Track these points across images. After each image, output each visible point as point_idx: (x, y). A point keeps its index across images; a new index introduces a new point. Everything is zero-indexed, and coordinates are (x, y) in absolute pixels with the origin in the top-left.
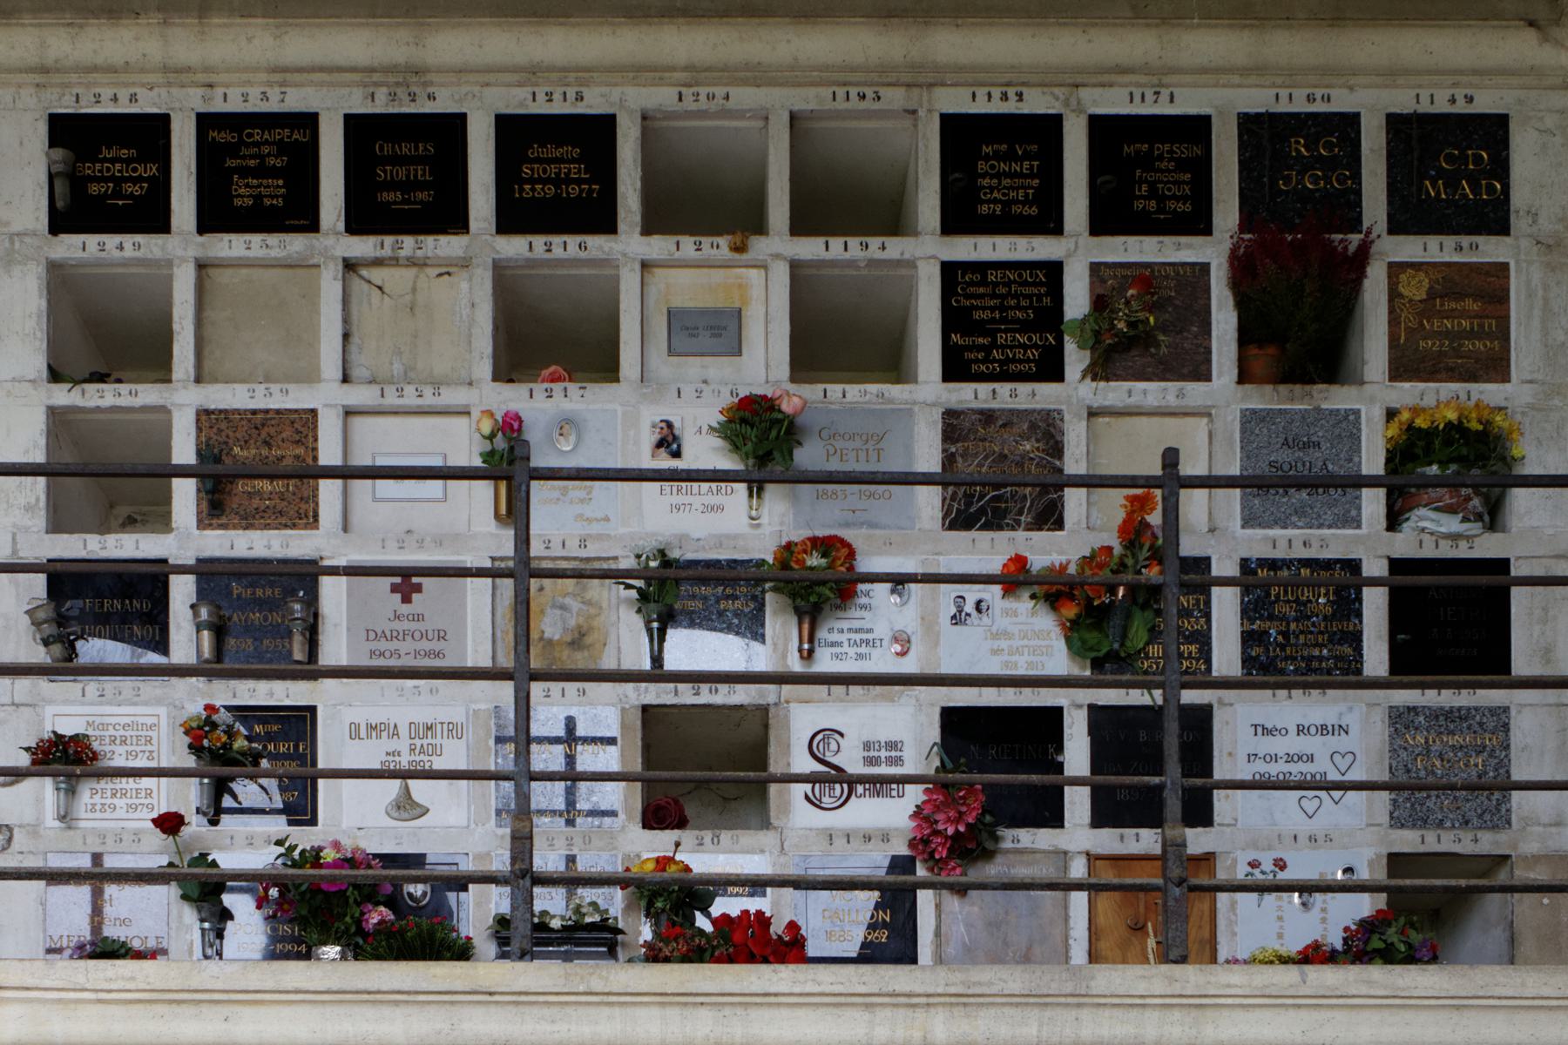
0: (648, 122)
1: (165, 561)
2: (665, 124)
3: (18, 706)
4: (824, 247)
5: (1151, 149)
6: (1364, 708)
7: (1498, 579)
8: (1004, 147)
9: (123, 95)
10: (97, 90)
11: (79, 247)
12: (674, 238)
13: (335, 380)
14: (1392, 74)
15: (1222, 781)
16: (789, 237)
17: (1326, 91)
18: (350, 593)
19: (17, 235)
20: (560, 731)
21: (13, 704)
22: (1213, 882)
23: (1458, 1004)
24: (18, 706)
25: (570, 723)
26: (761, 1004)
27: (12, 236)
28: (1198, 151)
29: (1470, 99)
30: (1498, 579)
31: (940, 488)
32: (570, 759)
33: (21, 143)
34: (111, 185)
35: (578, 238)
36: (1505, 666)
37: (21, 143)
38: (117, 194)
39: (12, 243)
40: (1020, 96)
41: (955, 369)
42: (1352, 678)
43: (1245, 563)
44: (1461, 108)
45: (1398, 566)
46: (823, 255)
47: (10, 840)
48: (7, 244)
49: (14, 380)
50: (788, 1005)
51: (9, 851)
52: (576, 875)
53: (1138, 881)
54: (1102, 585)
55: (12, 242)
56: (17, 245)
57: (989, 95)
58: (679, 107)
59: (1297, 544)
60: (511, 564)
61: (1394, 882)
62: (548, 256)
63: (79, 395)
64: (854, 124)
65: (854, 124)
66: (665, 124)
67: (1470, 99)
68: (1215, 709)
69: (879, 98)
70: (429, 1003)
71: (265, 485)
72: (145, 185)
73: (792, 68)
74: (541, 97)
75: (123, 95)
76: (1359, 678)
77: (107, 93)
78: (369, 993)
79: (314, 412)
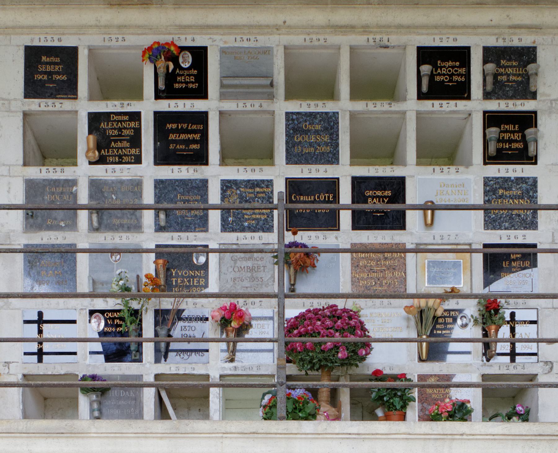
0: (288, 51)
1: (535, 246)
2: (363, 51)
3: (555, 309)
4: (366, 105)
9: (56, 37)
10: (124, 36)
11: (34, 104)
12: (366, 102)
13: (414, 165)
16: (349, 101)
17: (454, 36)
18: (90, 260)
19: (554, 100)
20: (36, 318)
21: (553, 308)
22: (140, 383)
23: (317, 435)
24: (555, 309)
25: (40, 314)
26: (317, 438)
27: (551, 101)
29: (520, 40)
31: (154, 211)
32: (40, 332)
33: (555, 60)
37: (555, 60)
39: (552, 104)
46: (431, 109)
47: (551, 368)
48: (549, 105)
49: (552, 164)
50: (231, 438)
51: (552, 373)
52: (142, 383)
53: (68, 382)
54: (302, 252)
55: (552, 104)
56: (554, 105)
58: (305, 44)
59: (512, 237)
60: (276, 247)
61: (484, 383)
62: (440, 109)
63: (170, 171)
64: (303, 51)
65: (303, 51)
66: (363, 51)
69: (125, 40)
70: (282, 438)
71: (257, 210)
74: (114, 40)
76: (129, 293)
77: (49, 38)
78: (373, 434)
79: (338, 179)
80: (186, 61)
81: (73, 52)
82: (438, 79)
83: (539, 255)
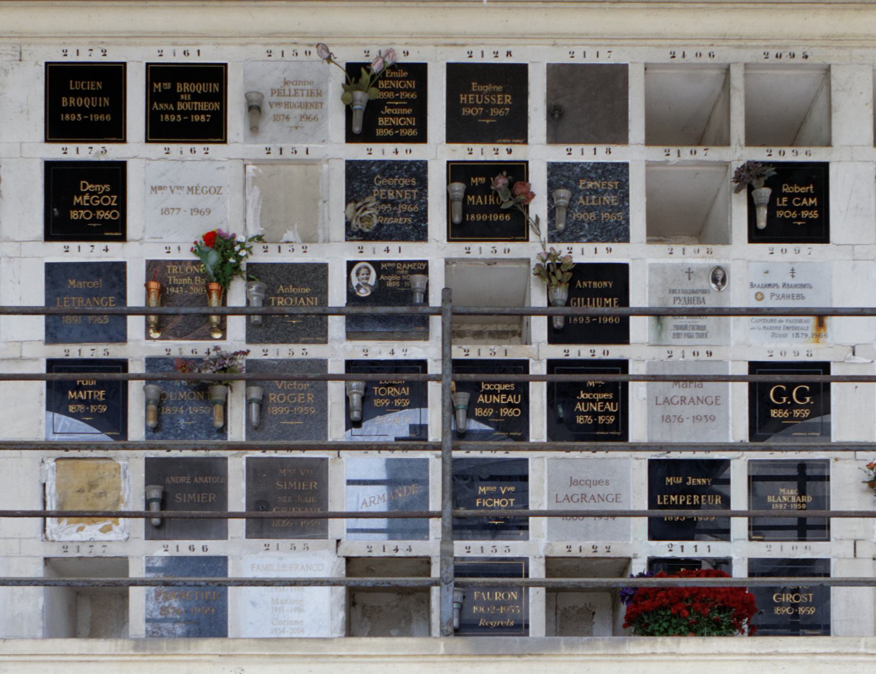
4: (593, 152)
5: (174, 87)
6: (53, 464)
7: (119, 376)
9: (180, 50)
14: (554, 39)
15: (535, 511)
26: (130, 661)
28: (216, 87)
30: (119, 376)
34: (482, 109)
35: (189, 146)
36: (625, 437)
38: (486, 115)
40: (767, 57)
41: (621, 234)
42: (423, 443)
43: (754, 367)
44: (503, 59)
45: (52, 364)
57: (684, 56)
68: (831, 464)
72: (508, 109)
73: (828, 37)
75: (193, 50)
81: (619, 73)
82: (780, 214)
83: (835, 388)
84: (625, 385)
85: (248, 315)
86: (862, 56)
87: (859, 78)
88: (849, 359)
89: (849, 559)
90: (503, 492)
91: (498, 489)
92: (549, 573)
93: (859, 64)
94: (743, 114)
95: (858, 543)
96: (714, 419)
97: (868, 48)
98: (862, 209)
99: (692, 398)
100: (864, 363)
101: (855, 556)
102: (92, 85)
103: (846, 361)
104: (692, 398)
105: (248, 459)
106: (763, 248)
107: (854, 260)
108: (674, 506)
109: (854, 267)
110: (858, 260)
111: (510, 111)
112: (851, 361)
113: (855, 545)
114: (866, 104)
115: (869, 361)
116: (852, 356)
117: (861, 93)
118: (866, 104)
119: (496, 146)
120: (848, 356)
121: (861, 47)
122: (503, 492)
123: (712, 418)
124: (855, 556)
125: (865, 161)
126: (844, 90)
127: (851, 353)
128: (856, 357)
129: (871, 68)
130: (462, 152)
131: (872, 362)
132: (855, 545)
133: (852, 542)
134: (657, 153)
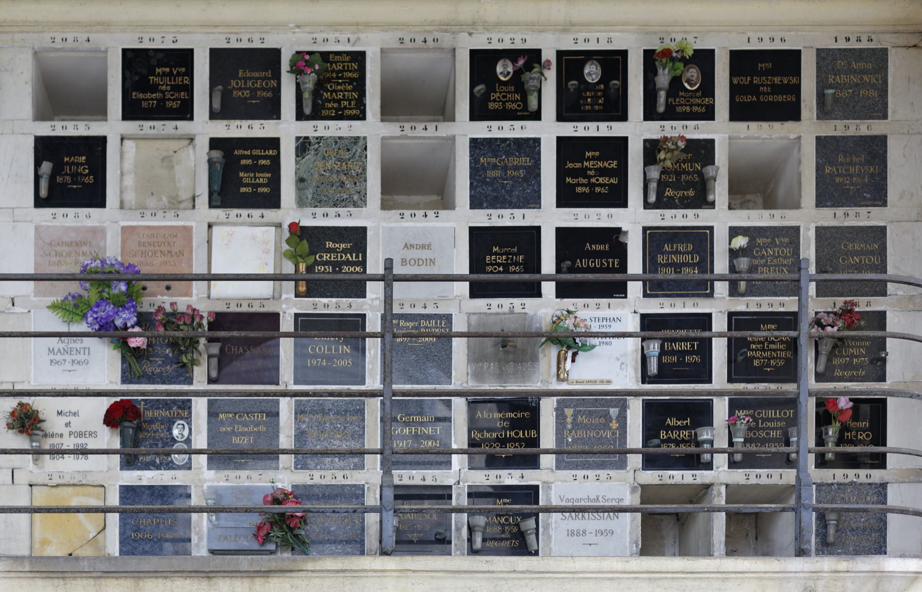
8: (168, 70)
9: (256, 37)
67: (610, 41)
72: (179, 102)
80: (592, 72)
81: (359, 58)
84: (472, 271)
85: (297, 281)
86: (23, 40)
87: (20, 59)
88: (9, 309)
89: (8, 485)
90: (175, 73)
91: (171, 71)
92: (122, 499)
93: (20, 47)
94: (727, 167)
95: (14, 471)
96: (88, 363)
97: (28, 32)
98: (21, 176)
99: (59, 349)
100: (22, 313)
101: (13, 482)
102: (180, 80)
103: (6, 311)
104: (59, 349)
105: (364, 384)
106: (47, 212)
107: (14, 221)
108: (681, 340)
109: (14, 228)
110: (17, 221)
111: (157, 103)
112: (11, 311)
113: (13, 472)
114: (26, 83)
115: (27, 311)
116: (12, 306)
117: (22, 73)
118: (26, 83)
119: (53, 123)
120: (8, 307)
121: (22, 32)
122: (175, 73)
123: (86, 361)
124: (13, 482)
125: (23, 134)
126: (6, 70)
127: (11, 304)
128: (15, 307)
129: (31, 50)
130: (614, 129)
131: (29, 311)
132: (13, 472)
133: (11, 470)
134: (391, 129)
